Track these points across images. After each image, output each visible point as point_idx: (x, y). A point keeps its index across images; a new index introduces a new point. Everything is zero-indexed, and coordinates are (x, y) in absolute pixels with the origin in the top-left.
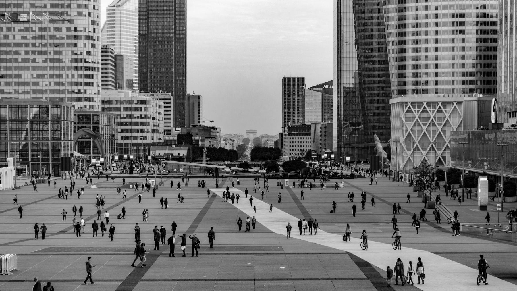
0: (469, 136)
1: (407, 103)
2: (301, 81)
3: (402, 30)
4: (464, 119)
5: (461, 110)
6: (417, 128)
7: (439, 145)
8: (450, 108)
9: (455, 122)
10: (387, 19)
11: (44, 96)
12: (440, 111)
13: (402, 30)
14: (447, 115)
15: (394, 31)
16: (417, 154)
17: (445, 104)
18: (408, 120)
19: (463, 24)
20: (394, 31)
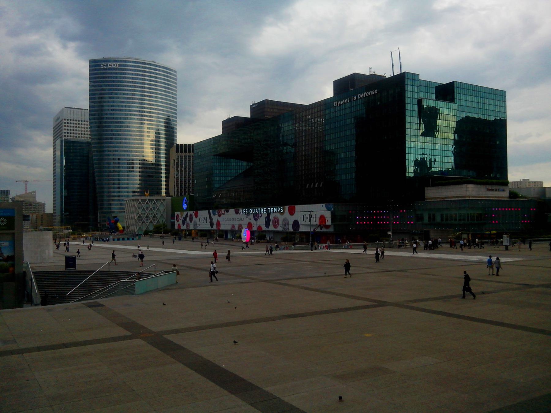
7: (154, 220)
9: (162, 209)
16: (144, 224)
17: (157, 200)
18: (139, 208)
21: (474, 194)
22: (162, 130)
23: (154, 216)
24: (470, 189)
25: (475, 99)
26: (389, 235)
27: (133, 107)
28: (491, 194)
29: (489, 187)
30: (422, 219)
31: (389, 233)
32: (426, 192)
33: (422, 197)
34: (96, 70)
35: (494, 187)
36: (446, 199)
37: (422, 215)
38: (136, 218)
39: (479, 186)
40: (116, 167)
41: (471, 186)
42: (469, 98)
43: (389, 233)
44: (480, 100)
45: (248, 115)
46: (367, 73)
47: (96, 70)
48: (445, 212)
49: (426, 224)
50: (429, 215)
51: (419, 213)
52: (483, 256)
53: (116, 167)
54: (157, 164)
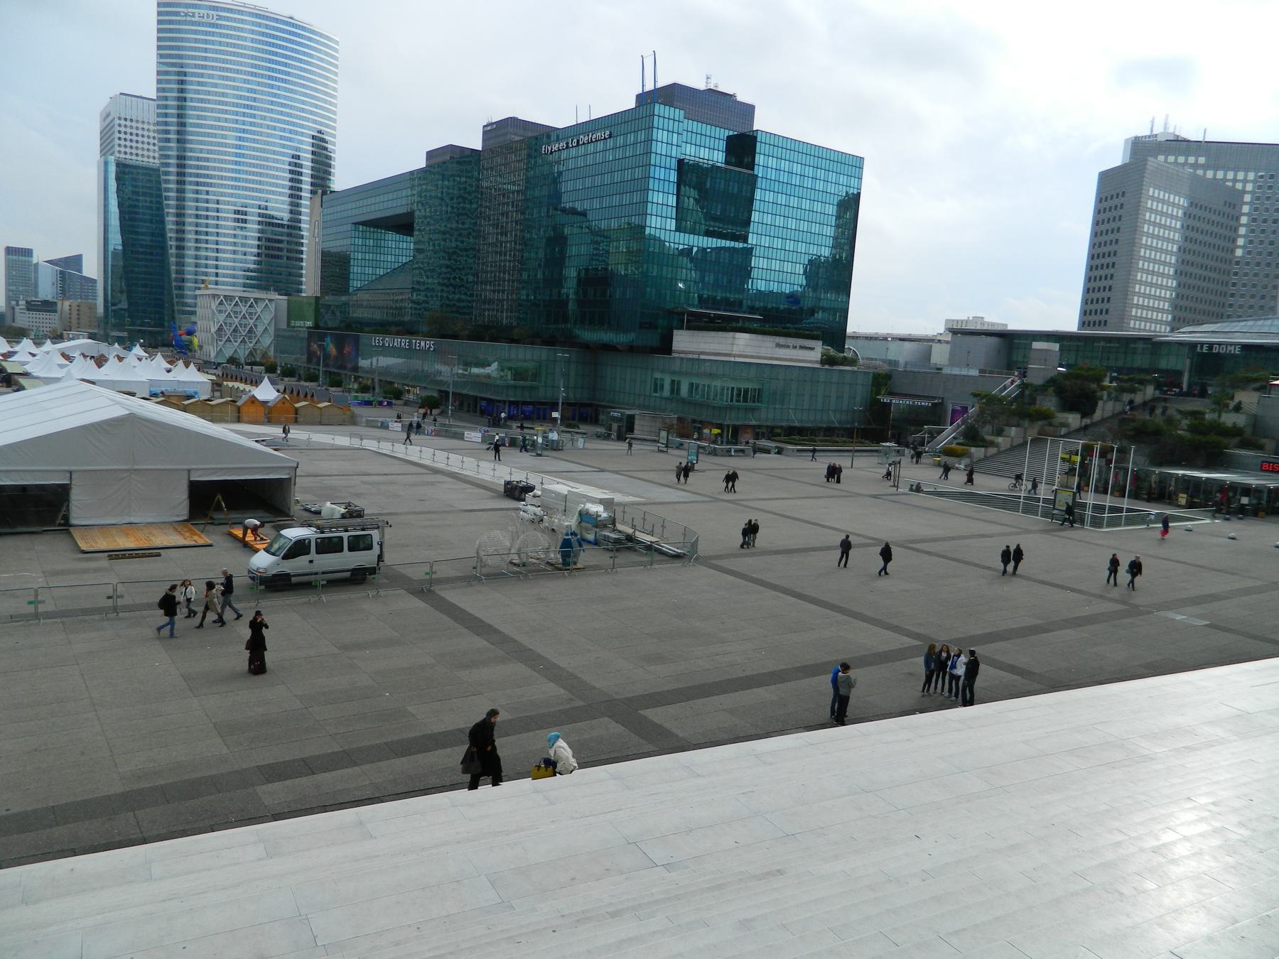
0: (597, 416)
1: (219, 296)
2: (28, 253)
3: (180, 235)
4: (275, 316)
5: (272, 307)
6: (229, 321)
7: (250, 338)
8: (262, 305)
9: (267, 318)
10: (167, 198)
11: (718, 384)
12: (236, 304)
13: (180, 235)
14: (259, 310)
15: (173, 243)
16: (228, 345)
17: (256, 300)
18: (220, 312)
19: (245, 221)
20: (173, 243)
21: (749, 351)
22: (306, 151)
23: (250, 331)
24: (742, 342)
25: (797, 168)
26: (555, 419)
27: (262, 101)
28: (783, 353)
29: (781, 340)
30: (662, 387)
31: (555, 415)
32: (675, 339)
33: (665, 347)
34: (168, 13)
35: (791, 341)
36: (702, 357)
37: (662, 380)
38: (213, 330)
39: (760, 337)
40: (213, 218)
41: (743, 338)
42: (785, 165)
43: (555, 415)
44: (809, 171)
45: (476, 143)
46: (701, 85)
47: (168, 13)
48: (695, 380)
49: (666, 399)
50: (673, 381)
51: (657, 375)
52: (43, 525)
53: (213, 218)
54: (294, 226)
